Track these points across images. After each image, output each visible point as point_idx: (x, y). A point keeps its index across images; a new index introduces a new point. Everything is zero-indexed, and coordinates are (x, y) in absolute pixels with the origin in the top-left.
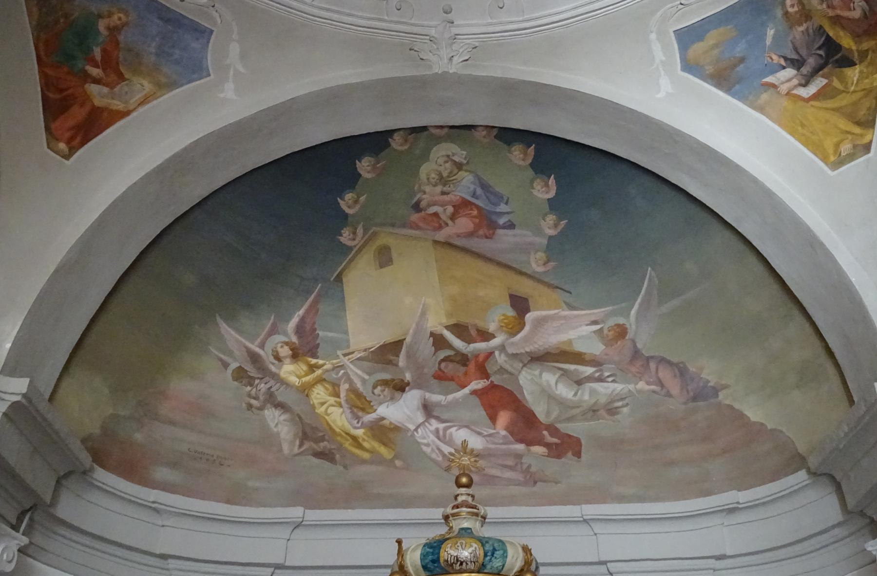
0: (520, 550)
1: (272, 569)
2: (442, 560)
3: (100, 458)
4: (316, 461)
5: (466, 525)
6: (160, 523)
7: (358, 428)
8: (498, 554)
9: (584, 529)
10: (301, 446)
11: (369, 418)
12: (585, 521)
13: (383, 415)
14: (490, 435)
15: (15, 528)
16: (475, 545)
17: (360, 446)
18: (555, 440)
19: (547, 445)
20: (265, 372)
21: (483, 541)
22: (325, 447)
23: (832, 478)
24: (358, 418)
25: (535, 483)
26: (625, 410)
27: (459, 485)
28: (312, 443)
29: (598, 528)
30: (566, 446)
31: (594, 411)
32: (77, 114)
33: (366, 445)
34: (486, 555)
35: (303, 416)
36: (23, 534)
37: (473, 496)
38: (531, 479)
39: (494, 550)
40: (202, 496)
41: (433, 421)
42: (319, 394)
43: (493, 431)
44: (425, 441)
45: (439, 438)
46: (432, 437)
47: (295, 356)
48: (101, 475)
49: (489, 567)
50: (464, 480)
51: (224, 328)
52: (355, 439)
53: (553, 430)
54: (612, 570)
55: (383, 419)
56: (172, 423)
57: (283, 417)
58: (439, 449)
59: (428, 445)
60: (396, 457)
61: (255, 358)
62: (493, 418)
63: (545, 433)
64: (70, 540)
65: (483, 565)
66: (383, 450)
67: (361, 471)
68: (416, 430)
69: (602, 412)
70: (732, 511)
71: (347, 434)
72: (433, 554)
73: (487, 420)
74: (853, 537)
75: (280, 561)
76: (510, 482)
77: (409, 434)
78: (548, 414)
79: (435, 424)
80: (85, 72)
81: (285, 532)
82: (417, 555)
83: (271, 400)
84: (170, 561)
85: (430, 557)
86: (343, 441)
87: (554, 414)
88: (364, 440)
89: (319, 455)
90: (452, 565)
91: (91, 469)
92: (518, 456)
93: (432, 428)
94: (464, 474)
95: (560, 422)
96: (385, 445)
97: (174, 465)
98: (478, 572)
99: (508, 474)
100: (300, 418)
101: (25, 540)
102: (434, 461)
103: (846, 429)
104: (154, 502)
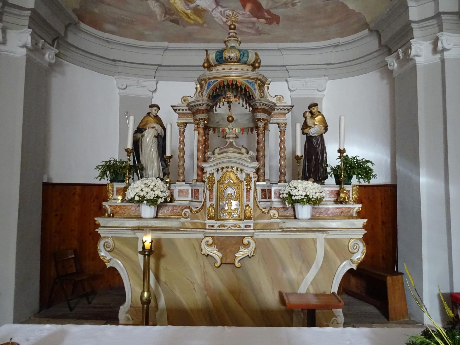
0: (254, 55)
1: (157, 67)
2: (223, 58)
3: (81, 18)
4: (171, 24)
5: (233, 45)
6: (111, 47)
7: (187, 10)
8: (246, 55)
9: (279, 53)
10: (165, 17)
11: (192, 5)
12: (279, 49)
13: (198, 4)
14: (243, 14)
15: (53, 46)
16: (236, 52)
17: (189, 18)
18: (270, 17)
19: (266, 19)
21: (239, 50)
22: (174, 18)
23: (378, 32)
24: (188, 5)
25: (260, 34)
26: (299, 4)
27: (230, 29)
28: (169, 16)
29: (284, 52)
31: (286, 4)
33: (191, 17)
34: (240, 56)
35: (165, 4)
36: (56, 48)
37: (236, 33)
38: (259, 33)
39: (244, 54)
40: (126, 37)
41: (220, 8)
43: (243, 12)
44: (216, 16)
45: (222, 15)
46: (219, 14)
48: (83, 26)
49: (242, 60)
50: (232, 27)
52: (187, 14)
53: (268, 12)
54: (288, 69)
55: (198, 6)
56: (109, 5)
57: (156, 4)
58: (221, 19)
59: (217, 18)
60: (204, 23)
62: (244, 7)
63: (265, 13)
64: (76, 52)
65: (240, 60)
66: (199, 20)
67: (189, 28)
68: (212, 11)
69: (290, 5)
70: (336, 46)
71: (184, 12)
72: (220, 55)
73: (242, 8)
74: (380, 56)
75: (159, 63)
76: (250, 34)
77: (210, 13)
78: (267, 4)
79: (220, 9)
81: (161, 52)
82: (214, 56)
84: (117, 62)
85: (219, 56)
86: (182, 15)
87: (270, 5)
88: (191, 15)
89: (172, 21)
90: (227, 59)
91: (78, 23)
92: (254, 23)
93: (219, 10)
94: (233, 24)
95: (272, 8)
96: (200, 17)
97: (113, 23)
98: (238, 62)
99: (250, 31)
100: (164, 5)
101: (57, 51)
102: (219, 24)
103: (388, 10)
104: (107, 38)
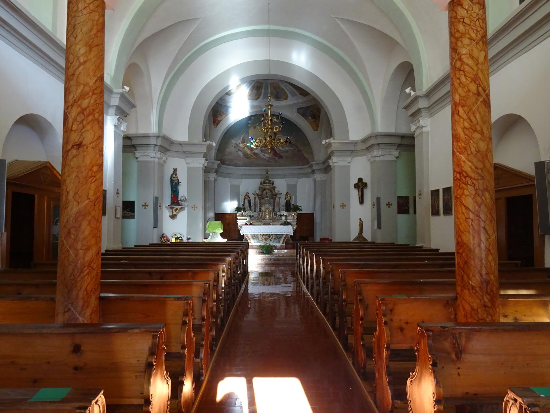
20: (238, 146)
30: (281, 157)
32: (217, 122)
42: (246, 148)
47: (242, 143)
51: (232, 141)
61: (236, 144)
80: (183, 375)
83: (239, 150)
